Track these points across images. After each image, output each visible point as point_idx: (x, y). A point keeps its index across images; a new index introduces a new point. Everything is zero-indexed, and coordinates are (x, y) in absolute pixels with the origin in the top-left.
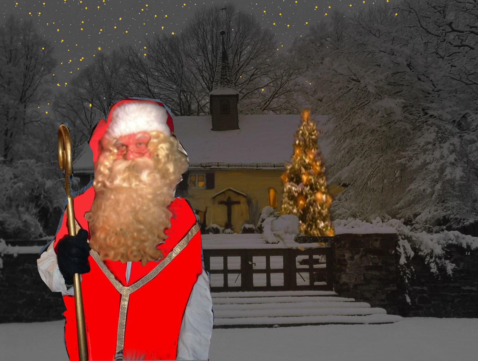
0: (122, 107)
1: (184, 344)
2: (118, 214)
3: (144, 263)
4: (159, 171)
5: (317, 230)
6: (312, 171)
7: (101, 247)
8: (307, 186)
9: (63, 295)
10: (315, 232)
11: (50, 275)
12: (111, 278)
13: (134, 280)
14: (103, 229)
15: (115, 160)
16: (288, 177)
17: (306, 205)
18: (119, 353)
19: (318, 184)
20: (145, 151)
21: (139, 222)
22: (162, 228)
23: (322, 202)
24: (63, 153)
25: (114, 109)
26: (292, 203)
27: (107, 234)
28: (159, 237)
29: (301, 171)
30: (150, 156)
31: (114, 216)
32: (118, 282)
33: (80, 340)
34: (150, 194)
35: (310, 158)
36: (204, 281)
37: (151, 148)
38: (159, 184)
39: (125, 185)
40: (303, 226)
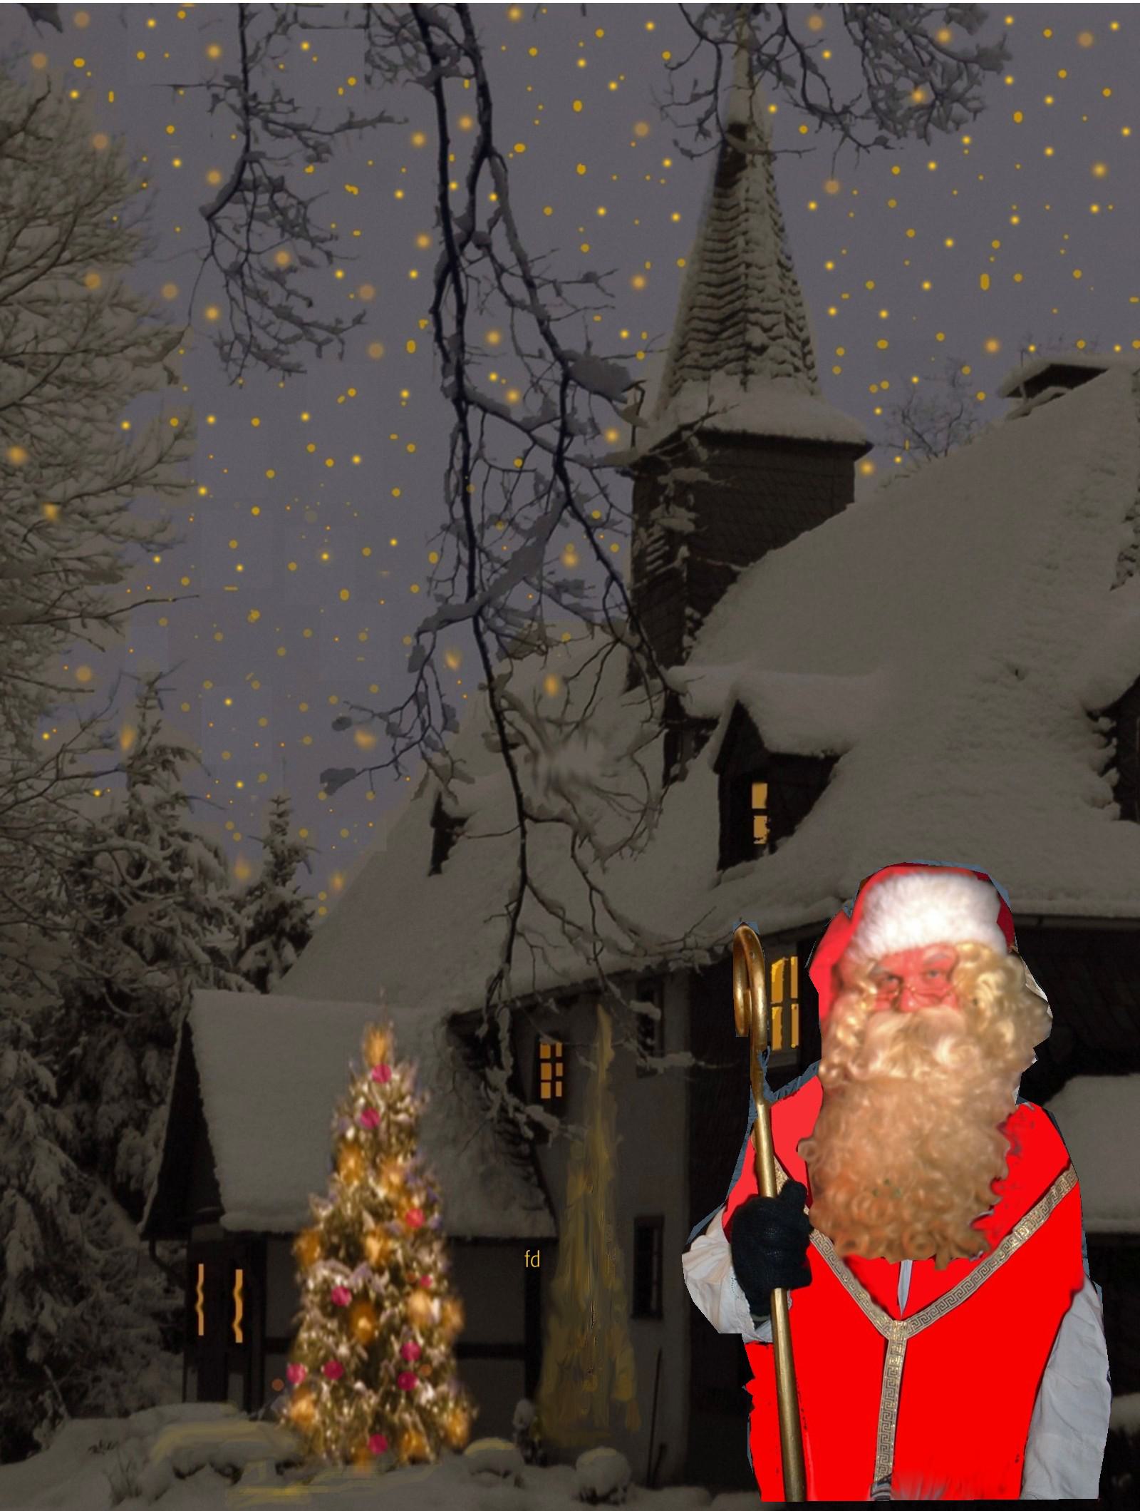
0: (890, 884)
1: (1039, 1460)
2: (879, 1144)
3: (942, 1263)
4: (979, 1039)
5: (414, 1411)
6: (397, 1224)
7: (837, 1225)
8: (379, 1271)
9: (745, 1341)
10: (407, 1417)
11: (715, 1293)
12: (863, 1299)
13: (918, 1303)
14: (844, 1180)
15: (871, 1014)
16: (322, 1245)
17: (377, 1333)
18: (881, 1482)
19: (415, 1265)
20: (945, 990)
21: (932, 1164)
22: (987, 1178)
23: (429, 1324)
24: (745, 996)
25: (871, 889)
26: (332, 1325)
27: (853, 1193)
28: (978, 1199)
29: (361, 1224)
30: (958, 1003)
31: (869, 1149)
32: (878, 1310)
33: (787, 1451)
34: (958, 1095)
35: (390, 1185)
36: (1087, 1305)
37: (959, 983)
38: (980, 1071)
39: (897, 1073)
40: (370, 1397)
